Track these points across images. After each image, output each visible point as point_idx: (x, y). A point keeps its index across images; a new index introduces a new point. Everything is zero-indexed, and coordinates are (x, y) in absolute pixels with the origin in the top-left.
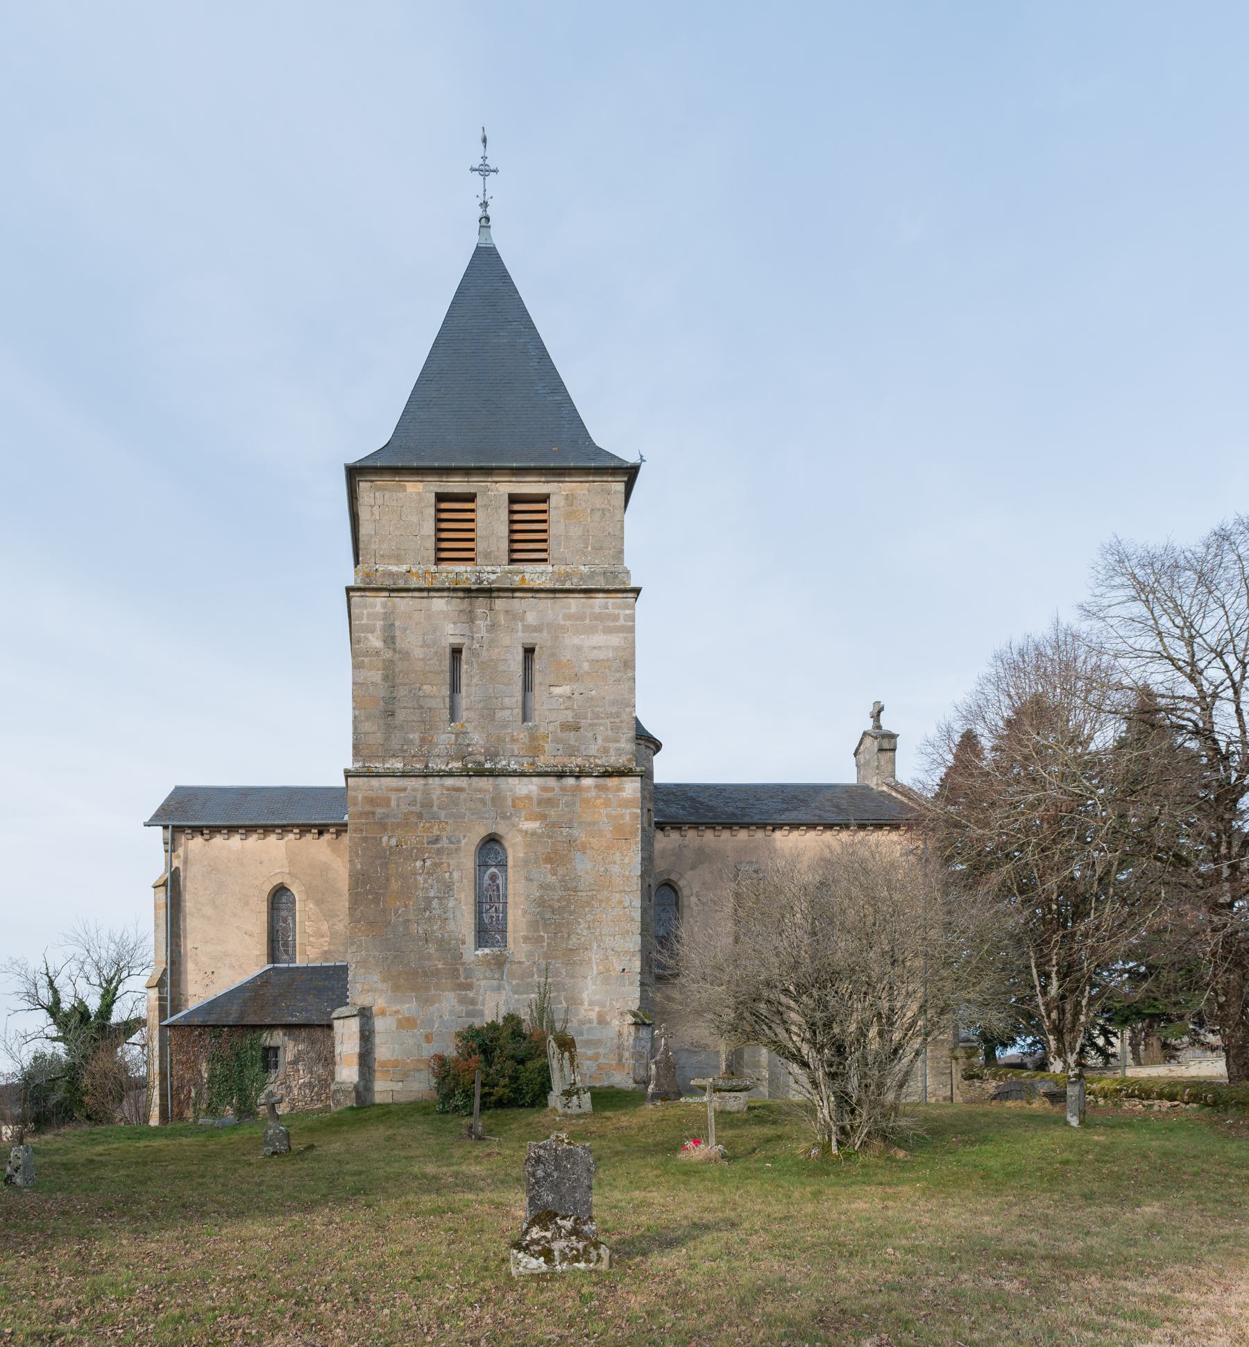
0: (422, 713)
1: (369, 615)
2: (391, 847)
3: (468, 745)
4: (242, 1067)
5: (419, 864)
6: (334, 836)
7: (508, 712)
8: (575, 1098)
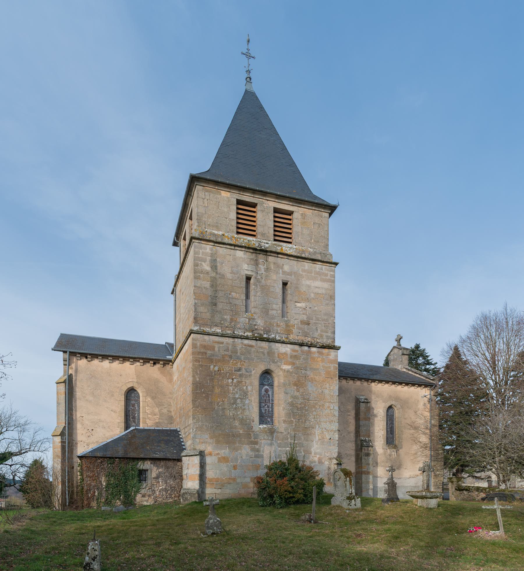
2: (215, 371)
3: (255, 325)
4: (127, 479)
5: (230, 381)
6: (162, 366)
7: (275, 312)
8: (353, 501)
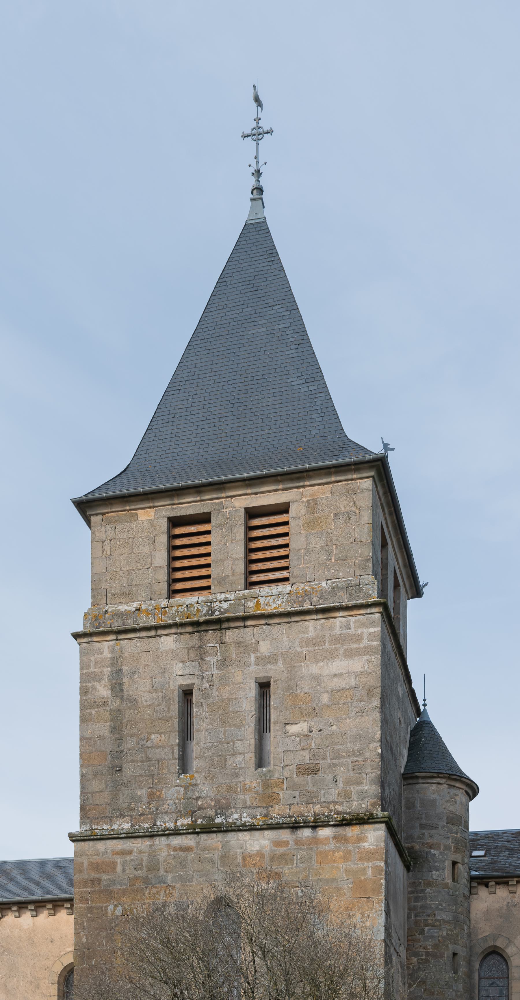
0: (150, 766)
1: (96, 661)
2: (117, 917)
3: (198, 799)
7: (239, 758)
